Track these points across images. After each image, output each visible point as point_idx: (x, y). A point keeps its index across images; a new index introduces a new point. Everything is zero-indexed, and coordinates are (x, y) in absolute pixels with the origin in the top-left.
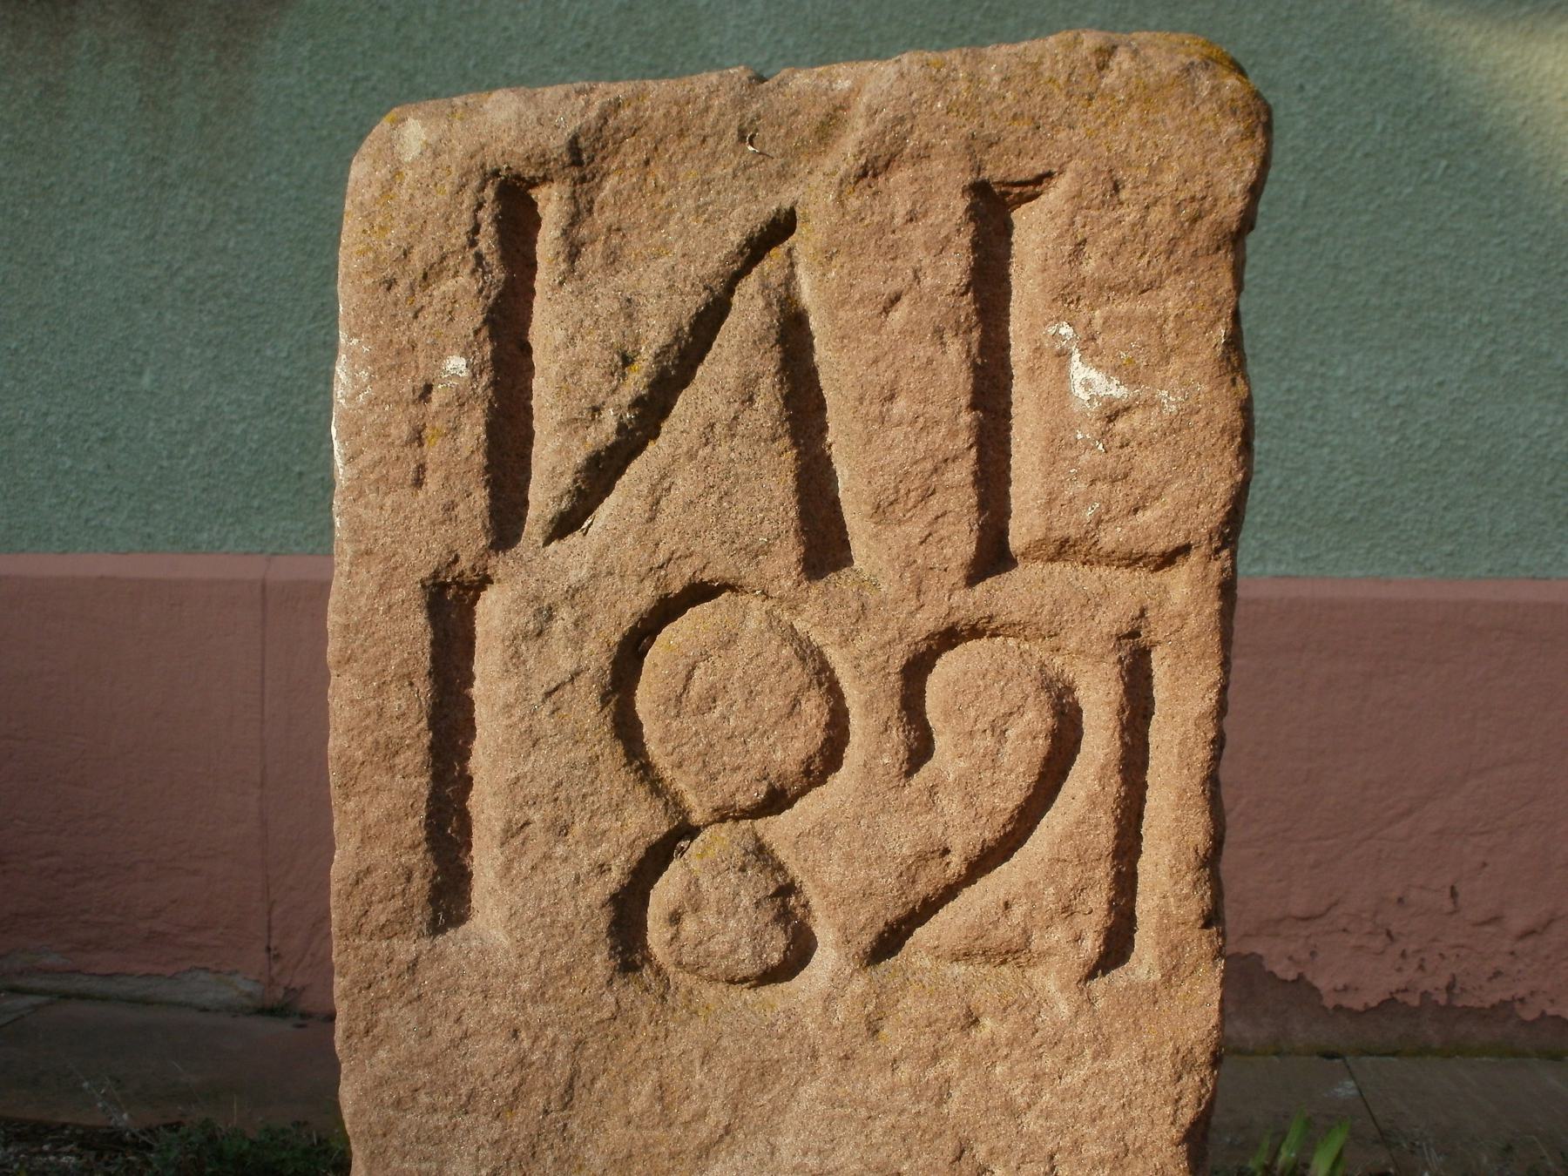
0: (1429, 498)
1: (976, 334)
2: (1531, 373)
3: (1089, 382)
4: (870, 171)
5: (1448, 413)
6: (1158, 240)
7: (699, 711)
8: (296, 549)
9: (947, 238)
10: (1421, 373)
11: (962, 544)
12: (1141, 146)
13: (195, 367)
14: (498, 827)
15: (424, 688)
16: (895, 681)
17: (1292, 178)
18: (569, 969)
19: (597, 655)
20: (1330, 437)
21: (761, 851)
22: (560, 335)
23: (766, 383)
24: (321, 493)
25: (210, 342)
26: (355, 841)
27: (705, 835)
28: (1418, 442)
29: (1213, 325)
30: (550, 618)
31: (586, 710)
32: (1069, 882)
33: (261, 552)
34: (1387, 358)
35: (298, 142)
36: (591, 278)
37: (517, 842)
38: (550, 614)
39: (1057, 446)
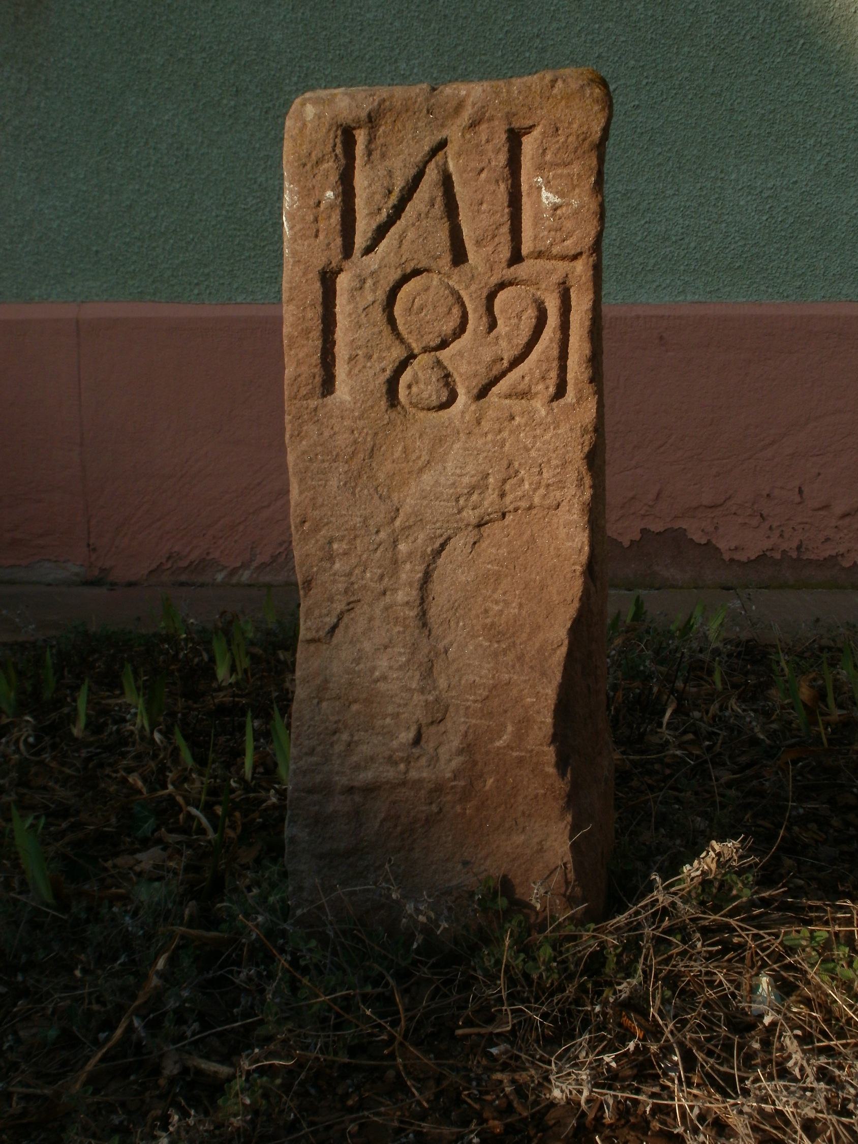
0: (787, 254)
1: (510, 182)
2: (852, 174)
3: (548, 197)
4: (474, 125)
5: (799, 201)
6: (571, 147)
7: (417, 314)
8: (97, 299)
9: (500, 149)
10: (783, 176)
11: (505, 253)
12: (566, 115)
13: (24, 185)
14: (346, 357)
15: (320, 309)
16: (484, 301)
17: (705, 55)
18: (372, 407)
19: (381, 295)
20: (726, 217)
21: (439, 362)
22: (366, 183)
23: (438, 199)
24: (110, 263)
25: (32, 170)
26: (295, 365)
27: (419, 357)
28: (780, 219)
29: (590, 177)
30: (364, 282)
31: (378, 314)
32: (544, 368)
33: (74, 301)
34: (763, 167)
35: (81, 37)
36: (376, 163)
37: (353, 362)
38: (364, 281)
39: (537, 219)
